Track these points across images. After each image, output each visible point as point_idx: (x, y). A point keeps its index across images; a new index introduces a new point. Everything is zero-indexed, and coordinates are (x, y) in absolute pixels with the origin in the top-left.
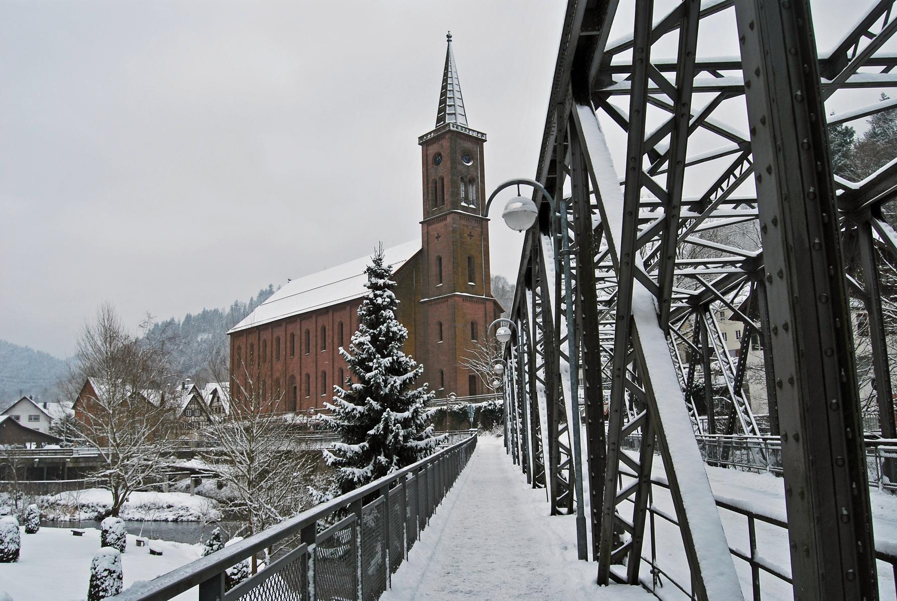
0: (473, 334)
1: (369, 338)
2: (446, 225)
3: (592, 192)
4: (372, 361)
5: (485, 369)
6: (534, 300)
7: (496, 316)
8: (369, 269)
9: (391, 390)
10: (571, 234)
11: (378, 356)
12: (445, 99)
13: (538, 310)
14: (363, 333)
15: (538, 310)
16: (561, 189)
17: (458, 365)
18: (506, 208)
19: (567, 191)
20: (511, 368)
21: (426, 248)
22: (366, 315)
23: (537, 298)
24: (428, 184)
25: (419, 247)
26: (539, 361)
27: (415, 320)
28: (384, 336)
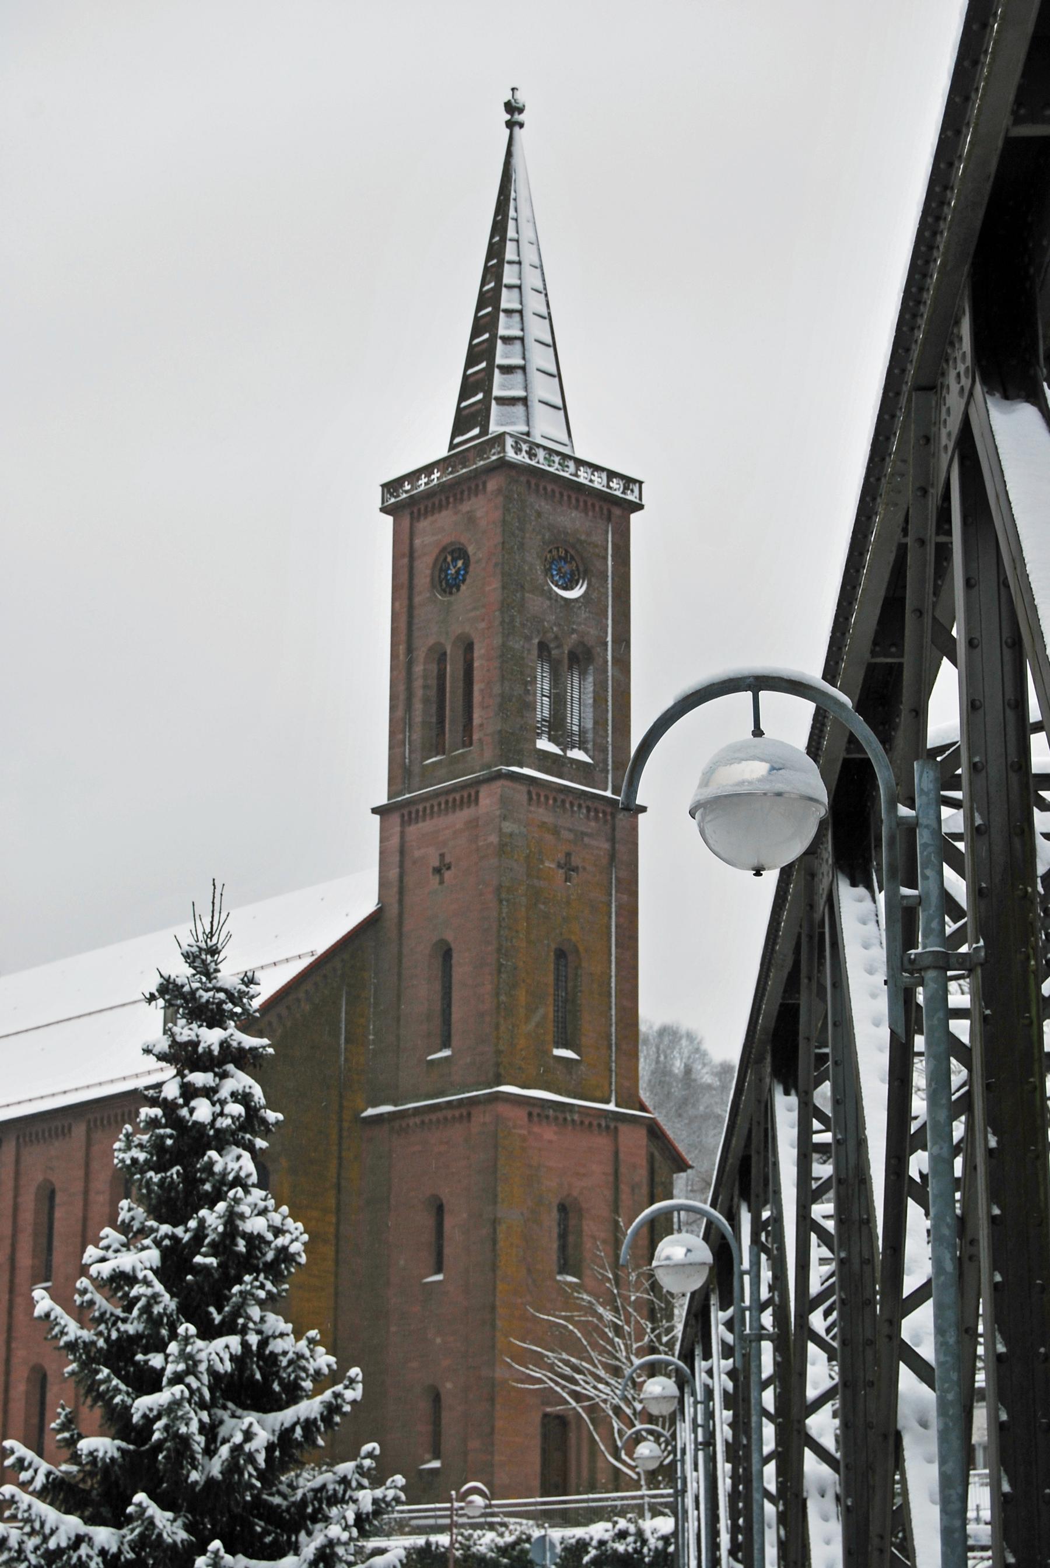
0: (563, 1248)
1: (153, 1256)
2: (473, 824)
3: (1038, 727)
4: (161, 1347)
5: (607, 1393)
6: (805, 1132)
7: (659, 1189)
8: (168, 989)
9: (232, 1467)
10: (956, 885)
11: (187, 1328)
12: (491, 344)
13: (822, 1170)
14: (133, 1235)
15: (822, 1170)
16: (920, 714)
17: (500, 1373)
18: (705, 782)
19: (944, 716)
20: (709, 1393)
21: (393, 910)
22: (148, 1165)
23: (816, 1125)
24: (410, 664)
25: (364, 903)
26: (820, 1373)
27: (339, 1188)
28: (216, 1249)
